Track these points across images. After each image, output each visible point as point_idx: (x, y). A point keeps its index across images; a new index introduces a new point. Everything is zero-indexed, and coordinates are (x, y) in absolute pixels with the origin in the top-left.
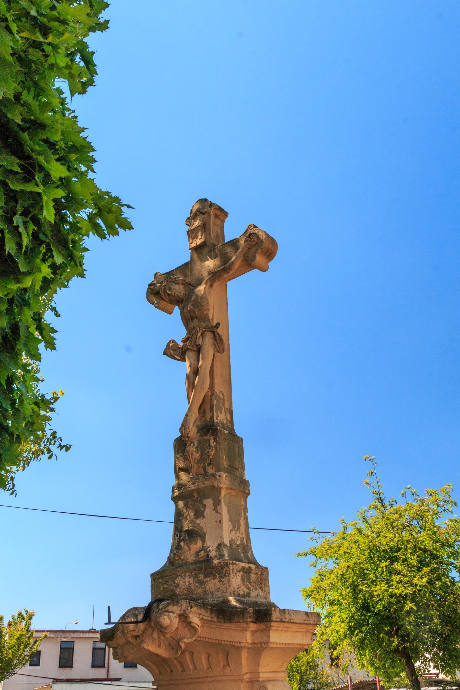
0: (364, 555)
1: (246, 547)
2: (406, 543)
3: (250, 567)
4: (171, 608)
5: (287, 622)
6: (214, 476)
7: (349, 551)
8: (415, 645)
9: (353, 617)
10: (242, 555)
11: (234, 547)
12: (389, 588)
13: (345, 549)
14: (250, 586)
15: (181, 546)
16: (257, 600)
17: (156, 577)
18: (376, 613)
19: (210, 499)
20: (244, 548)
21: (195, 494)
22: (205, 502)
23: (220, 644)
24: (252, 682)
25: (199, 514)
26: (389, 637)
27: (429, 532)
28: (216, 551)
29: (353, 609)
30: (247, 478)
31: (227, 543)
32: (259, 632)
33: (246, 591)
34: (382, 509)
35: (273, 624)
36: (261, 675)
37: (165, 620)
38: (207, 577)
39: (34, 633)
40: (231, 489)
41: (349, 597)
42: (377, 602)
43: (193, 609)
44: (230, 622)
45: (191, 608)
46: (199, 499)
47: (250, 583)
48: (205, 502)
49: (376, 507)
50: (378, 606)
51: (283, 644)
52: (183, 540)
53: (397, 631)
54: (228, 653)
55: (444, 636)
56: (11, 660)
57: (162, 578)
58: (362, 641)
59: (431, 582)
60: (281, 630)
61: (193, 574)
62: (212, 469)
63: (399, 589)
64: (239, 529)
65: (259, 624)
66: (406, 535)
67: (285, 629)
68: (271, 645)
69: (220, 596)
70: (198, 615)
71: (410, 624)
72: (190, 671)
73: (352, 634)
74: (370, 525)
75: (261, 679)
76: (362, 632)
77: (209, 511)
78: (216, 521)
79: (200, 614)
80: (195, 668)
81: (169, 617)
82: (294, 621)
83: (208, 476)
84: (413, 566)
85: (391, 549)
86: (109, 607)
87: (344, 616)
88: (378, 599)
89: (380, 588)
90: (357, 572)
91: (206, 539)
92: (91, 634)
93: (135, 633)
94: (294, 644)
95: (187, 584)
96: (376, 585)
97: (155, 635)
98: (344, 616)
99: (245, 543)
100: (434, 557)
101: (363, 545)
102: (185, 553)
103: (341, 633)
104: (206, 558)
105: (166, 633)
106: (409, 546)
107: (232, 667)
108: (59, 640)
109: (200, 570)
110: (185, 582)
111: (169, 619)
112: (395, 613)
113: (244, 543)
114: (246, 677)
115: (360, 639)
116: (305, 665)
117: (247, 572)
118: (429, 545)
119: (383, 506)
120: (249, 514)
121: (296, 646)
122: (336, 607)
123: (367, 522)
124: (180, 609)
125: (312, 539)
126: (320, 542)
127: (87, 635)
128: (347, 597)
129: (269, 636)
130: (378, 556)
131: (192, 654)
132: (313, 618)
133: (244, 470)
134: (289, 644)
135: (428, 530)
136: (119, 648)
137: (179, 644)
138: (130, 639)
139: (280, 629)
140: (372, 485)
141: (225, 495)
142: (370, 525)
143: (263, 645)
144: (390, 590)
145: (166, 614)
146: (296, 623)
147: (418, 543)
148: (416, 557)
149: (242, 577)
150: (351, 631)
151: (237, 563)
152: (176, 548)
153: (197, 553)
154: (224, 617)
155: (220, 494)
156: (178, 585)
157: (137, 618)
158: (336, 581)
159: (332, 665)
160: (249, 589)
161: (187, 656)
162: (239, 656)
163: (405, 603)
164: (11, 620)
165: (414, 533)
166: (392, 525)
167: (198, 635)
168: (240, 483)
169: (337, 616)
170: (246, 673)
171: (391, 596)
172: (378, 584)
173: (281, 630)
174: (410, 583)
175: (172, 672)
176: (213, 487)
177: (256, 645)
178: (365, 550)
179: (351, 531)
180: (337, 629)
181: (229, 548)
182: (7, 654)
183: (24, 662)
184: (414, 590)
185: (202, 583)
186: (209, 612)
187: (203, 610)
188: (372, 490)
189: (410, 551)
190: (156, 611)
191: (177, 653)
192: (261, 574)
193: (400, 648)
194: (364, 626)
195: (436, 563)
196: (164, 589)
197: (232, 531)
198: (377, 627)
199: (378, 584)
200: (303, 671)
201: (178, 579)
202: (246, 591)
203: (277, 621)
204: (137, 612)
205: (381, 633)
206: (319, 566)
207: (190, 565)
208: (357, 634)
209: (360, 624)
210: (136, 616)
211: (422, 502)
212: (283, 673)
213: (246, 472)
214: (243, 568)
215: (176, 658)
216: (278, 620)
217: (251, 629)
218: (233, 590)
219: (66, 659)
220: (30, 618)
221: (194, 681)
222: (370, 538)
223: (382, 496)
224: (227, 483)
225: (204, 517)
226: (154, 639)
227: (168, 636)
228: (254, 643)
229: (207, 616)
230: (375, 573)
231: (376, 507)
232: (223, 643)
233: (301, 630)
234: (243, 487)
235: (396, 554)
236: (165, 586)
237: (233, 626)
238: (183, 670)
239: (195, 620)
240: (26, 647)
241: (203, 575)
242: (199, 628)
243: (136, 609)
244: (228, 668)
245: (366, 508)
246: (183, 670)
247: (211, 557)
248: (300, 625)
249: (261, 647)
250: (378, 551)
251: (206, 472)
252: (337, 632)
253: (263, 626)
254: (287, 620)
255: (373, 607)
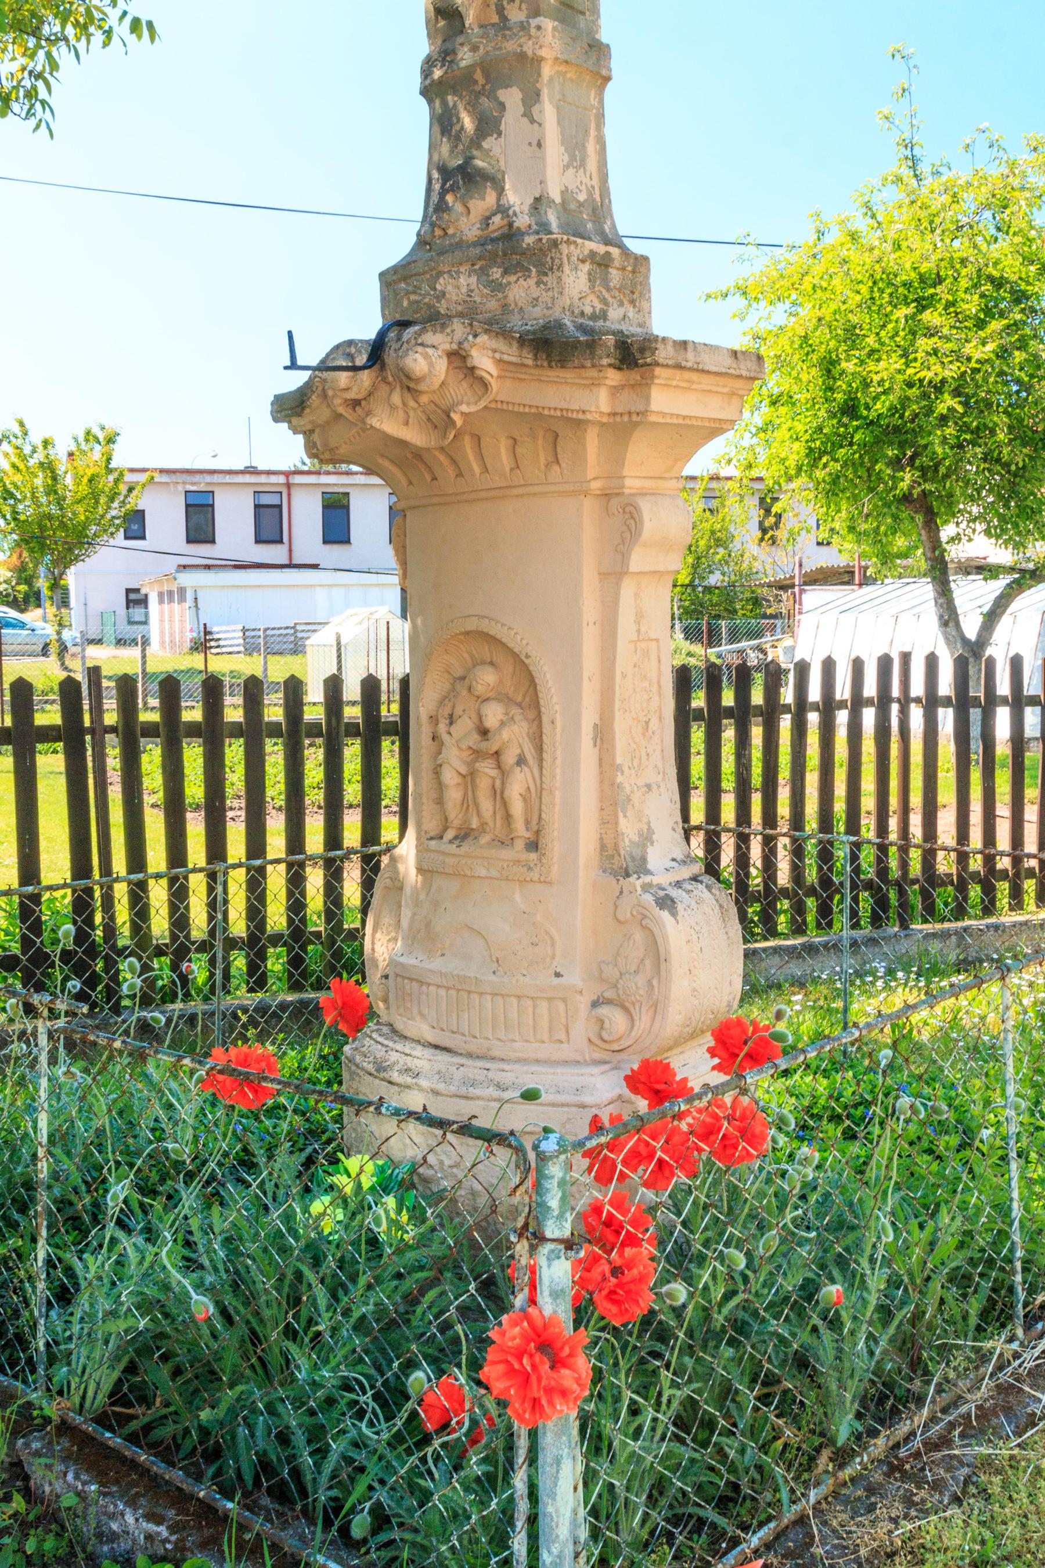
0: (858, 292)
1: (599, 209)
2: (958, 266)
3: (608, 253)
4: (429, 338)
5: (691, 369)
6: (524, 27)
7: (824, 284)
8: (948, 485)
9: (820, 429)
10: (589, 226)
11: (573, 206)
12: (908, 366)
13: (816, 281)
14: (607, 296)
15: (446, 204)
16: (623, 327)
17: (392, 280)
18: (872, 422)
19: (515, 88)
20: (594, 210)
21: (479, 76)
22: (503, 95)
23: (540, 416)
24: (606, 496)
25: (488, 126)
26: (894, 471)
27: (1018, 239)
28: (531, 215)
29: (822, 413)
30: (604, 37)
31: (556, 196)
32: (626, 390)
33: (599, 306)
34: (914, 182)
35: (658, 371)
36: (628, 482)
37: (417, 362)
38: (511, 274)
39: (126, 473)
40: (566, 62)
41: (815, 385)
42: (876, 399)
43: (479, 340)
44: (562, 367)
45: (475, 336)
46: (487, 87)
47: (608, 289)
48: (503, 95)
49: (899, 180)
50: (878, 406)
51: (678, 416)
52: (453, 189)
53: (912, 459)
54: (557, 435)
55: (1013, 468)
56: (85, 526)
57: (405, 279)
58: (835, 479)
59: (1003, 353)
60: (676, 387)
61: (477, 267)
62: (520, 9)
63: (929, 369)
64: (583, 164)
65: (627, 373)
66: (960, 247)
67: (684, 385)
68: (653, 418)
69: (538, 316)
70: (490, 354)
71: (944, 440)
72: (474, 475)
73: (814, 465)
74: (879, 223)
75: (626, 491)
76: (837, 460)
77: (512, 119)
78: (530, 144)
79: (495, 351)
80: (485, 470)
81: (426, 356)
82: (706, 368)
83: (509, 29)
84: (968, 318)
85: (922, 279)
86: (290, 333)
87: (800, 428)
88: (880, 389)
89: (888, 366)
90: (839, 332)
91: (507, 187)
92: (248, 476)
93: (352, 395)
94: (702, 419)
95: (464, 290)
96: (878, 360)
97: (396, 398)
98: (800, 428)
99: (598, 199)
100: (1019, 297)
101: (859, 269)
102: (457, 220)
103: (791, 463)
104: (505, 230)
105: (421, 392)
106: (964, 272)
107: (564, 465)
108: (180, 488)
109: (492, 259)
110: (459, 285)
111: (426, 360)
112: (912, 421)
113: (594, 200)
114: (596, 486)
115: (830, 474)
116: (706, 537)
117: (602, 263)
118: (1012, 268)
119: (916, 176)
120: (608, 131)
121: (707, 424)
122: (783, 410)
123: (873, 216)
124: (449, 339)
125: (740, 258)
126: (756, 266)
127: (240, 479)
128: (811, 387)
129: (648, 399)
130: (891, 295)
131: (478, 439)
132: (749, 364)
133: (599, 16)
134: (690, 417)
135: (1015, 234)
136: (317, 431)
137: (449, 416)
138: (341, 410)
139: (674, 383)
140: (897, 123)
141: (551, 79)
142: (879, 223)
143: (634, 418)
144: (910, 371)
145: (420, 349)
146: (708, 372)
147: (987, 265)
148: (977, 297)
149: (590, 274)
150: (814, 457)
151: (579, 241)
152: (436, 209)
153: (486, 220)
154: (548, 356)
155: (539, 75)
156: (444, 294)
157: (353, 361)
158: (790, 351)
159: (762, 539)
160: (604, 301)
161: (468, 443)
162: (581, 441)
163: (937, 398)
164: (73, 447)
165: (979, 239)
166: (931, 222)
167: (492, 397)
168: (587, 48)
169: (785, 427)
170: (595, 479)
171: (910, 385)
172: (884, 357)
173: (676, 387)
174: (958, 356)
175: (434, 479)
176: (522, 56)
177: (618, 419)
178: (861, 282)
179: (834, 237)
180: (783, 455)
181: (559, 208)
182: (74, 514)
183: (112, 529)
184: (963, 369)
185: (497, 287)
186: (515, 344)
187: (501, 339)
188: (895, 137)
189: (964, 283)
190: (394, 346)
191: (445, 436)
192: (634, 272)
193: (916, 492)
194: (841, 447)
195: (1023, 311)
196: (411, 303)
197: (566, 167)
198: (872, 449)
199: (884, 357)
200: (700, 550)
201: (441, 280)
202: (599, 306)
203: (667, 366)
204: (353, 350)
205: (877, 461)
206: (751, 321)
207: (469, 247)
208: (825, 466)
209: (833, 444)
210: (351, 357)
211: (1013, 165)
212: (674, 481)
213: (603, 21)
214: (593, 254)
215: (442, 449)
216: (670, 362)
217: (609, 382)
218: (568, 302)
219: (200, 522)
220: (110, 440)
221: (484, 494)
222: (876, 252)
223: (917, 151)
224: (557, 44)
225: (500, 134)
226: (393, 408)
227: (424, 399)
228: (615, 414)
229: (511, 353)
230: (877, 334)
231: (899, 180)
232: (546, 412)
233: (720, 389)
234: (593, 59)
235: (932, 291)
236: (413, 297)
237: (568, 375)
238: (460, 474)
239: (483, 361)
240: (112, 500)
241: (500, 270)
242: (493, 382)
243: (350, 343)
244: (556, 468)
245: (876, 182)
246: (460, 474)
247: (518, 228)
248: (718, 378)
249: (630, 421)
250: (890, 284)
251: (504, 18)
252: (783, 461)
253: (634, 376)
254: (689, 365)
255: (868, 408)
